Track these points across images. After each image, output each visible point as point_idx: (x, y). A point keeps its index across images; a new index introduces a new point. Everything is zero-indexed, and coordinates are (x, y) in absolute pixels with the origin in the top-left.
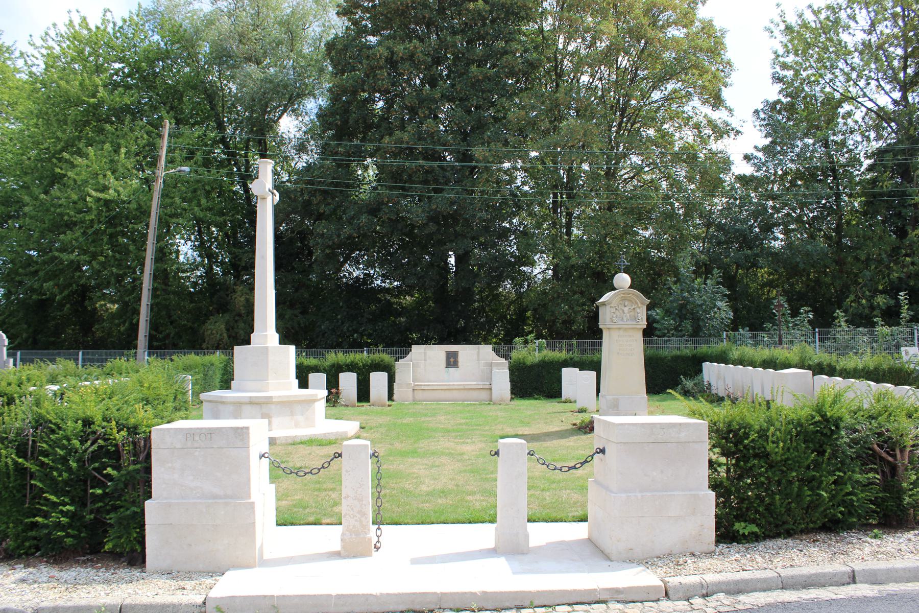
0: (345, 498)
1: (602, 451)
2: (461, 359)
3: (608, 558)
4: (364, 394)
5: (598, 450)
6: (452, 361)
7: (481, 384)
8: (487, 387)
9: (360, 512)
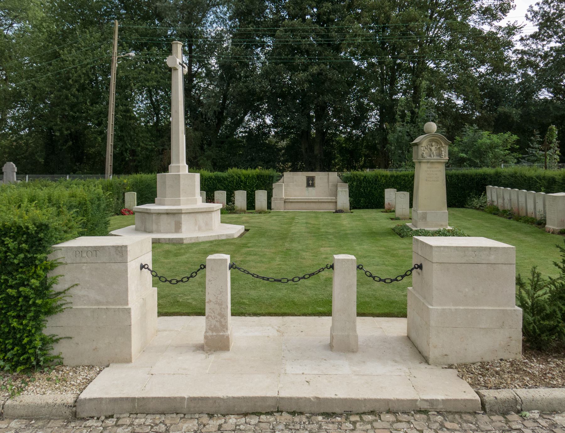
0: (208, 302)
1: (420, 267)
2: (317, 181)
3: (426, 360)
4: (251, 204)
5: (416, 266)
6: (310, 183)
7: (330, 198)
8: (334, 201)
9: (220, 314)
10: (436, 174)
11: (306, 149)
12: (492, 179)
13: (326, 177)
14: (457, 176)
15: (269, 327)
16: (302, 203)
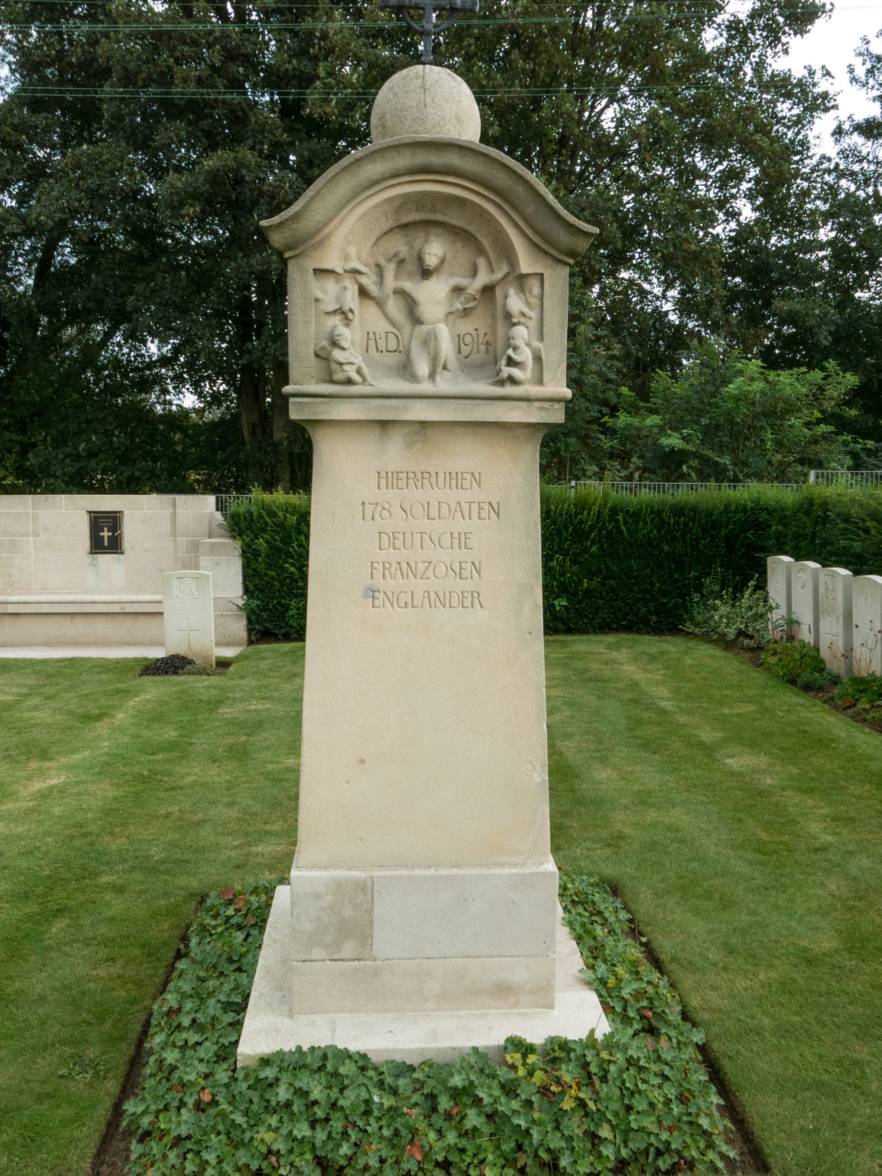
2: (130, 531)
10: (463, 540)
11: (253, 425)
12: (786, 526)
14: (656, 512)
16: (58, 619)
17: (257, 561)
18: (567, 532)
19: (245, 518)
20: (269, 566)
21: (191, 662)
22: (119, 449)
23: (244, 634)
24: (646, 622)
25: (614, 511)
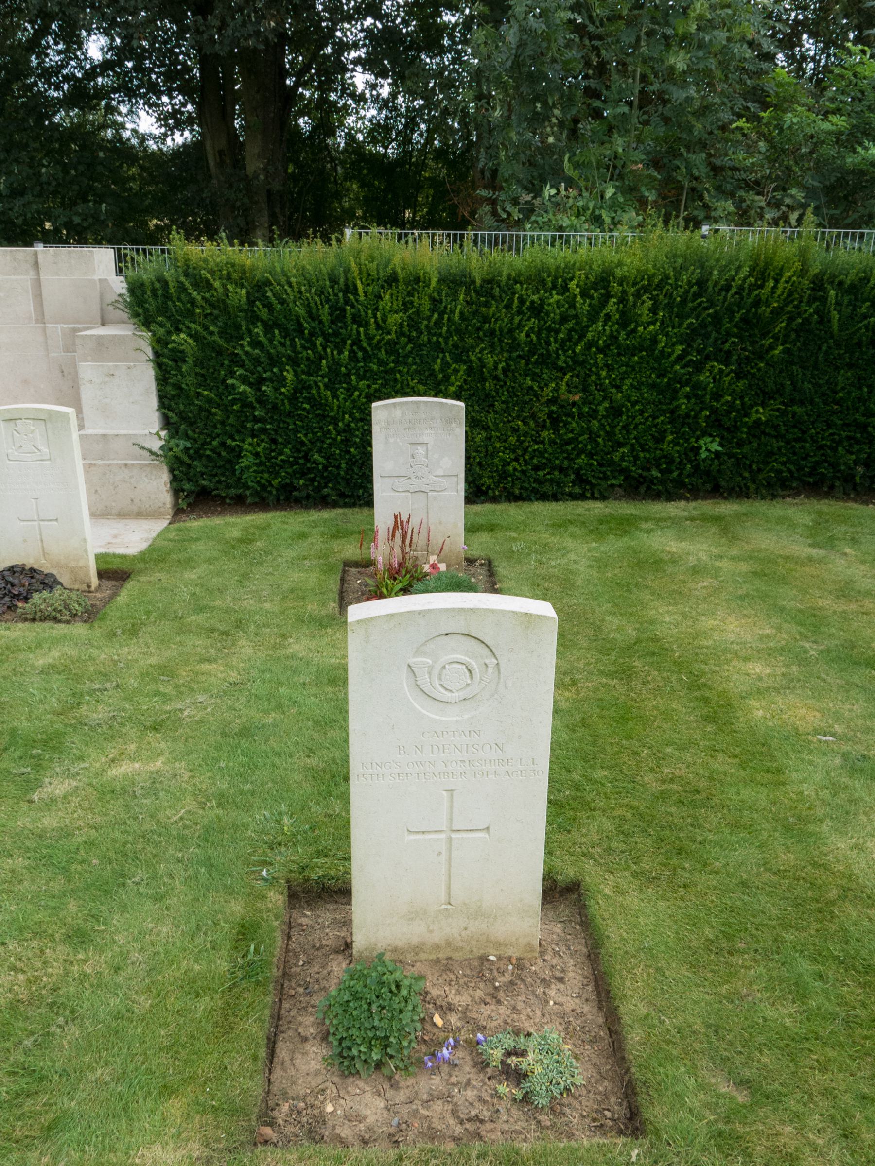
11: (221, 153)
13: (26, 279)
15: (194, 926)
17: (179, 369)
18: (731, 319)
19: (154, 291)
20: (203, 380)
21: (48, 582)
22: (49, 184)
23: (165, 498)
24: (848, 479)
25: (819, 284)
